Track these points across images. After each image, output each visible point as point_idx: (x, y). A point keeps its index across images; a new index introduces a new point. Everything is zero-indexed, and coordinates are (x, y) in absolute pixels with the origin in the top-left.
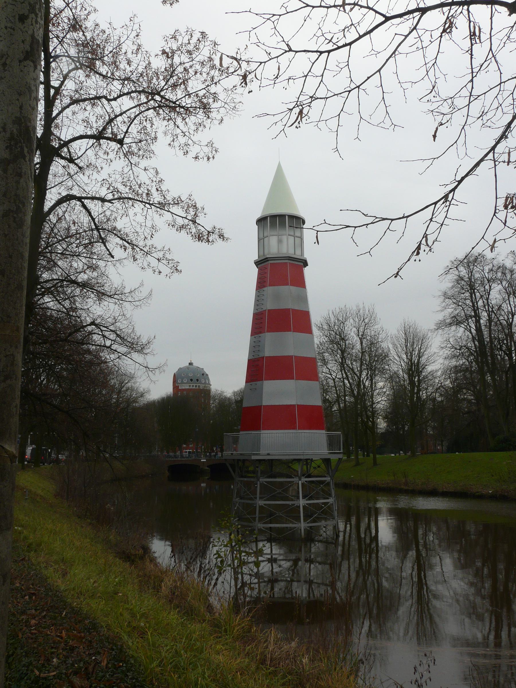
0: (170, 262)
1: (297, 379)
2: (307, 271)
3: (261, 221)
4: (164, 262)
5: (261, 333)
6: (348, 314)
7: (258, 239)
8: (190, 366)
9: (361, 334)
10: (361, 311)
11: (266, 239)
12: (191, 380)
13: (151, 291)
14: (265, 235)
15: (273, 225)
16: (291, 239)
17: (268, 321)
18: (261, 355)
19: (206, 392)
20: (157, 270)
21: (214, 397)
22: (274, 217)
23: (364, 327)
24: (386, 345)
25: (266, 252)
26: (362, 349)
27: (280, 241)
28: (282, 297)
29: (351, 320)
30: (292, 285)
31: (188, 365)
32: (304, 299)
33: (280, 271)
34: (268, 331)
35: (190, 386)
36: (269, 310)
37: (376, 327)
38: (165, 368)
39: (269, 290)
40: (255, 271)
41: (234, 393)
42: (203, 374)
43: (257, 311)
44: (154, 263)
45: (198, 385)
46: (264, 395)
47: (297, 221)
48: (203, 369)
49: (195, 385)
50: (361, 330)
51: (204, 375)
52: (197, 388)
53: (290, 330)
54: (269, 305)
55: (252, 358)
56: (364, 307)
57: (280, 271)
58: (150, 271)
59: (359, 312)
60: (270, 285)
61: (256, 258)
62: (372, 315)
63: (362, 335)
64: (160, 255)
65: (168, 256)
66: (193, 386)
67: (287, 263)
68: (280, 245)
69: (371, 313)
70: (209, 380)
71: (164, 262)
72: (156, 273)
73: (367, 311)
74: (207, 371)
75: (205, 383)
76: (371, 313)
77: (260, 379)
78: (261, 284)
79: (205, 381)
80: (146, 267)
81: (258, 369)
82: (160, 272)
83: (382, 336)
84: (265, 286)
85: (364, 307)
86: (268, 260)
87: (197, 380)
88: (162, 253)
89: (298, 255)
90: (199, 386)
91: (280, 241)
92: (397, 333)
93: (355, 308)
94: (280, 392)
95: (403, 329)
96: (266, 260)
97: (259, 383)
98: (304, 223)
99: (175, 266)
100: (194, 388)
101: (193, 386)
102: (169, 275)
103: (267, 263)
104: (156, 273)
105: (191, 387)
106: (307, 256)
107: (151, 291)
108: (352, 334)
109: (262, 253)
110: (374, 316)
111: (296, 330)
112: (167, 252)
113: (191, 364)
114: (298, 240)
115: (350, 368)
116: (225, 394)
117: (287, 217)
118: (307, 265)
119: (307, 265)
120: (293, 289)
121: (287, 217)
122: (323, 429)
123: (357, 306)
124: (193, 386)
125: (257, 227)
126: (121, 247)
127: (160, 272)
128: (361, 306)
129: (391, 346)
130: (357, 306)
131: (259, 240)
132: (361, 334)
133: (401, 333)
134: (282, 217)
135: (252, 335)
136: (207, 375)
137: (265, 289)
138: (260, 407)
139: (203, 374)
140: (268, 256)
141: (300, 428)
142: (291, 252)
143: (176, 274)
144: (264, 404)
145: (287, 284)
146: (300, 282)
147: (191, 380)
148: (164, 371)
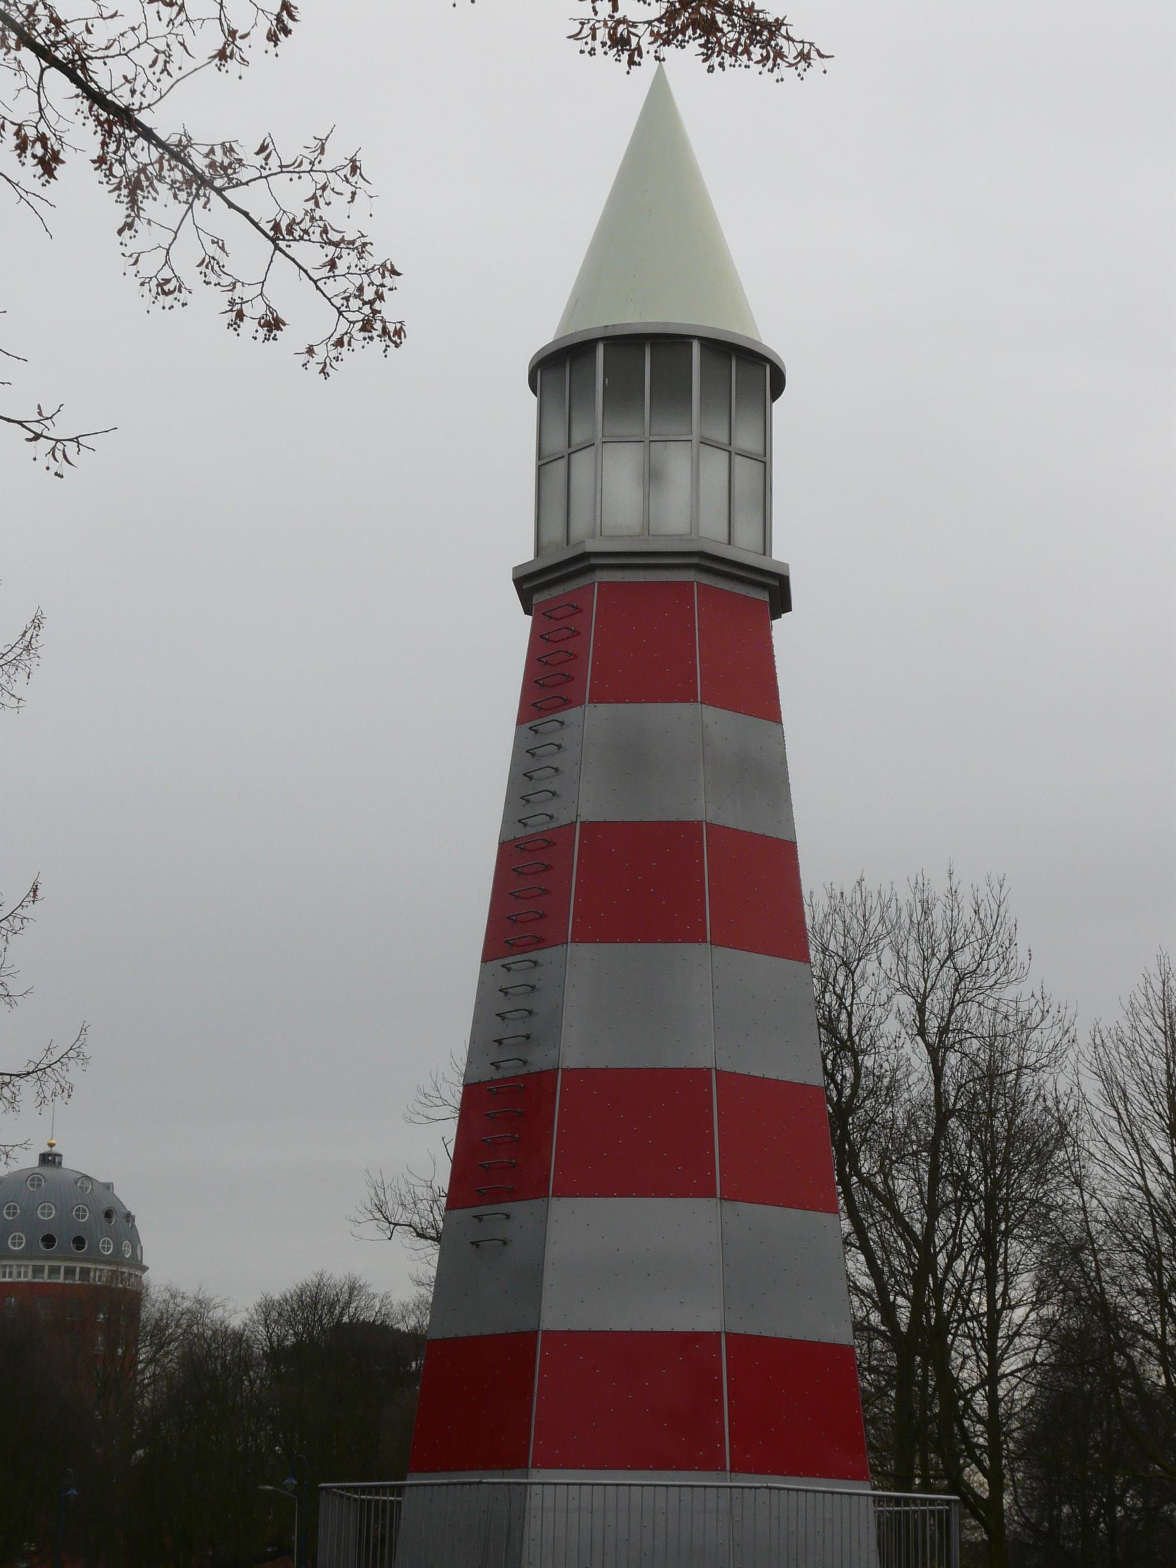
0: (348, 259)
1: (731, 1195)
2: (784, 632)
3: (558, 367)
4: (312, 254)
5: (541, 943)
6: (874, 920)
7: (540, 455)
8: (48, 1171)
9: (933, 1025)
10: (937, 913)
11: (582, 462)
12: (49, 1240)
13: (37, 623)
14: (578, 437)
15: (622, 395)
16: (716, 462)
17: (572, 882)
18: (539, 1061)
19: (121, 1302)
20: (256, 310)
21: (159, 1327)
22: (626, 345)
23: (949, 988)
24: (1066, 1084)
25: (581, 526)
26: (939, 1095)
27: (652, 477)
28: (651, 759)
29: (888, 958)
30: (709, 700)
31: (34, 1162)
32: (771, 779)
33: (649, 630)
34: (583, 936)
35: (38, 1270)
36: (590, 828)
37: (1009, 993)
38: (73, 1073)
39: (592, 722)
40: (513, 630)
41: (267, 1307)
42: (108, 1214)
43: (520, 832)
44: (248, 254)
45: (78, 1266)
46: (550, 1277)
47: (750, 373)
48: (108, 1186)
49: (63, 1265)
50: (936, 1003)
51: (115, 1218)
52: (77, 1280)
53: (695, 936)
54: (591, 799)
55: (487, 1073)
56: (953, 893)
57: (649, 630)
58: (209, 302)
59: (926, 912)
60: (597, 698)
61: (525, 554)
62: (993, 931)
63: (943, 1031)
64: (292, 197)
65: (336, 214)
66: (54, 1271)
67: (690, 584)
68: (658, 493)
69: (989, 925)
70: (135, 1240)
71: (312, 254)
72: (249, 326)
73: (967, 914)
74: (128, 1198)
75: (117, 1259)
76: (989, 925)
77: (531, 1186)
78: (547, 690)
79: (118, 1246)
80: (191, 276)
81: (519, 1134)
82: (273, 324)
83: (1043, 1037)
84: (568, 703)
85: (953, 893)
86: (593, 568)
87: (79, 1242)
88: (306, 187)
89: (744, 549)
90: (85, 1272)
91: (652, 477)
92: (1125, 1025)
93: (905, 896)
94: (633, 1264)
95: (1157, 1005)
96: (581, 564)
97: (522, 1210)
98: (778, 383)
99: (369, 294)
100: (61, 1279)
101: (54, 1271)
102: (321, 353)
103: (583, 581)
104: (249, 326)
105: (45, 1278)
106: (785, 551)
107: (37, 623)
108: (891, 1026)
109: (555, 532)
110: (1004, 937)
111: (736, 935)
112: (336, 182)
113: (49, 1159)
114: (745, 470)
115: (877, 1194)
116: (217, 1314)
117: (696, 347)
118: (790, 610)
119: (790, 610)
120: (719, 722)
121: (696, 347)
122: (857, 1475)
123: (919, 886)
124: (54, 1271)
125: (533, 400)
126: (22, 147)
127: (273, 324)
128: (938, 888)
129: (1093, 1087)
130: (919, 886)
131: (544, 462)
132: (933, 1025)
133: (1147, 1022)
134: (669, 345)
135: (490, 954)
136: (129, 1217)
137: (571, 715)
138: (519, 1346)
139: (108, 1214)
140: (592, 546)
141: (739, 1466)
142: (711, 533)
143: (367, 354)
144: (557, 1315)
145: (686, 696)
146: (753, 689)
147: (49, 1240)
148: (68, 1091)
